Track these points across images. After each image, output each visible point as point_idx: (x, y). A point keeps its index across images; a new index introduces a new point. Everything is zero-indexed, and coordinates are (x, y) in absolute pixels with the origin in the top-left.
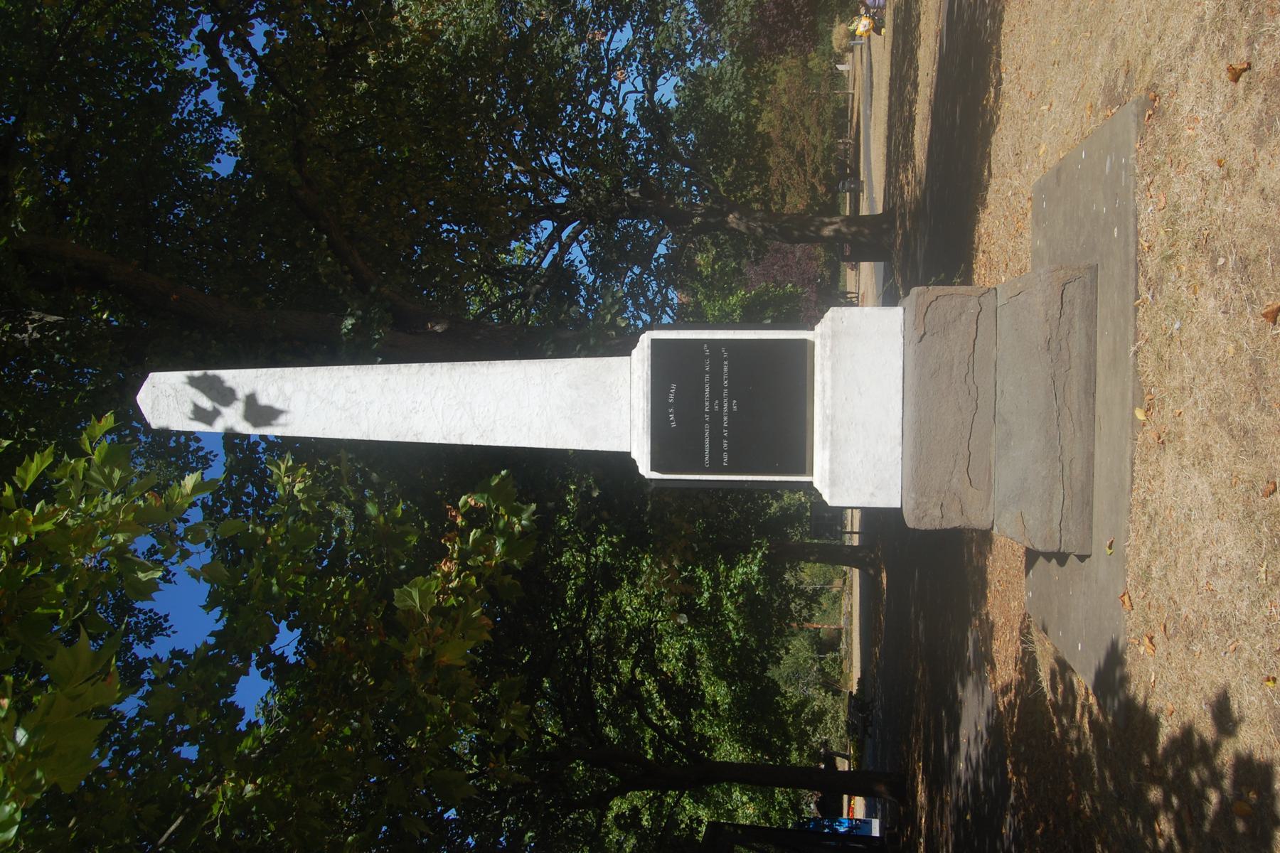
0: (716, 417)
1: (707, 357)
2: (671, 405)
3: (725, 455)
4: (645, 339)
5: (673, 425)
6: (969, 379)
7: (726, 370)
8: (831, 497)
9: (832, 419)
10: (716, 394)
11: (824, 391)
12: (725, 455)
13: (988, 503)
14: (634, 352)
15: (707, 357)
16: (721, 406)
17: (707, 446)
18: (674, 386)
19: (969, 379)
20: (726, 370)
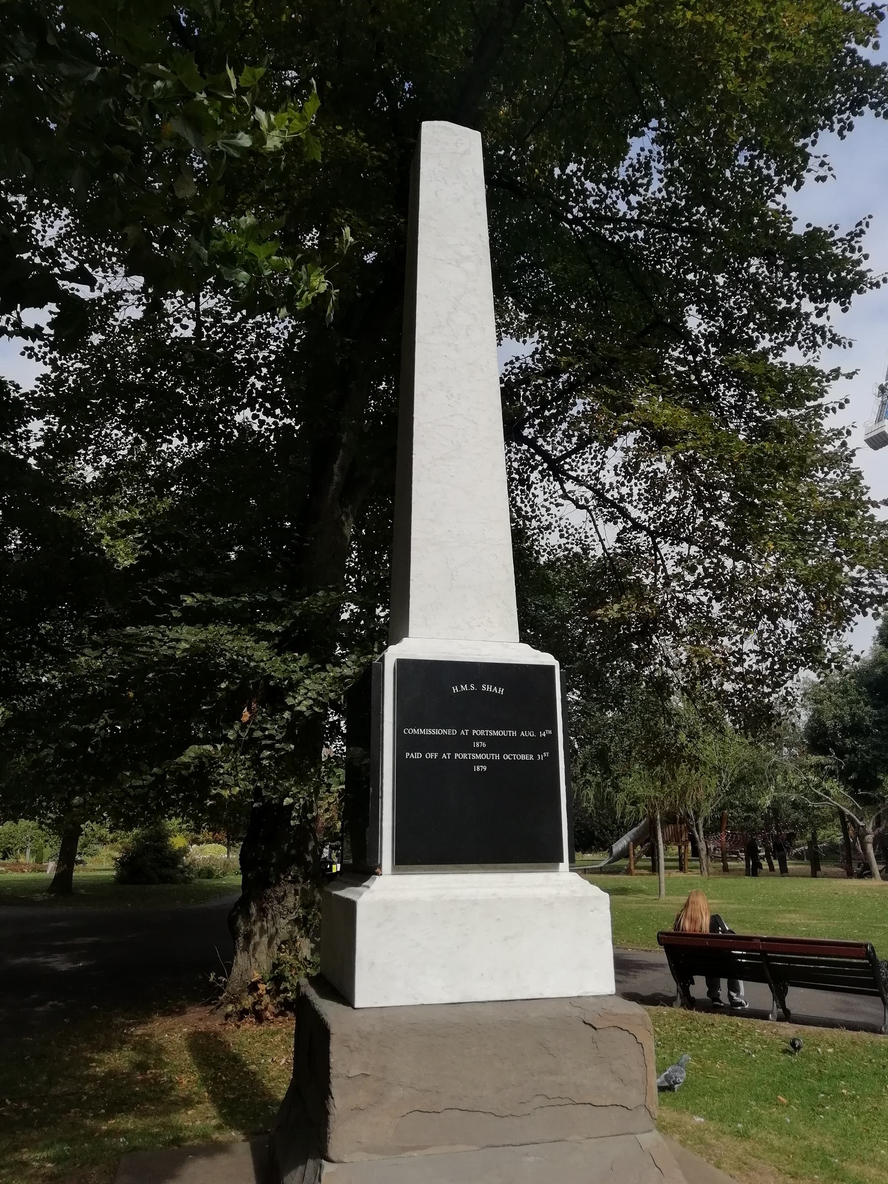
0: (465, 744)
1: (537, 734)
2: (478, 686)
3: (417, 756)
4: (547, 659)
5: (455, 689)
6: (538, 1101)
7: (523, 757)
8: (388, 907)
9: (838, 938)
10: (494, 744)
11: (636, 902)
12: (417, 756)
13: (367, 1150)
14: (526, 646)
15: (537, 734)
16: (480, 750)
17: (436, 732)
18: (501, 691)
19: (538, 1101)
20: (523, 757)
